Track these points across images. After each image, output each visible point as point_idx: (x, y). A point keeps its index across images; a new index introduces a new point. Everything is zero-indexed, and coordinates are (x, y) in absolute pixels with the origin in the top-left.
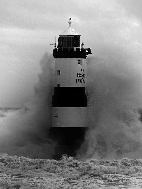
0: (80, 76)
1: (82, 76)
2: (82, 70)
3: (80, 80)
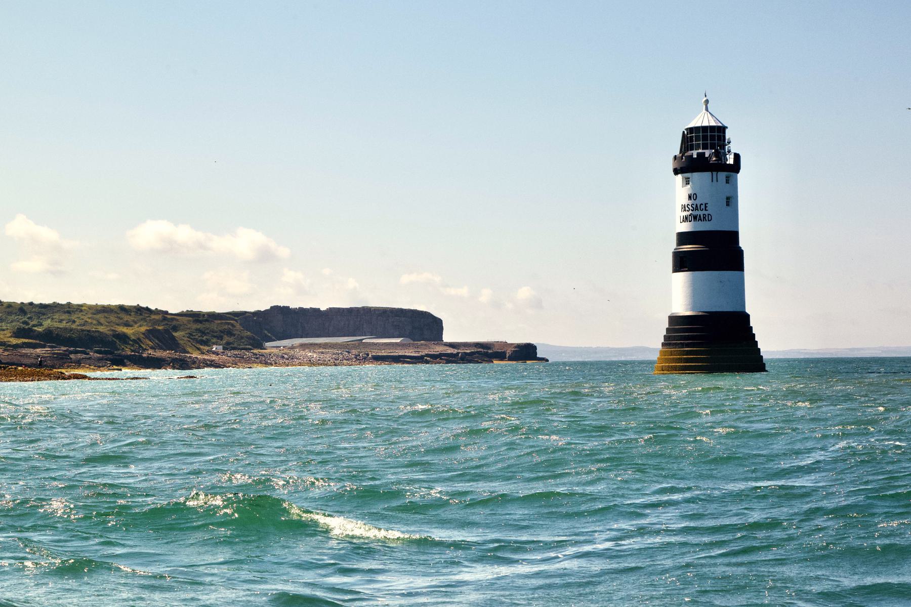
0: (687, 209)
1: (691, 208)
2: (690, 197)
3: (686, 218)
